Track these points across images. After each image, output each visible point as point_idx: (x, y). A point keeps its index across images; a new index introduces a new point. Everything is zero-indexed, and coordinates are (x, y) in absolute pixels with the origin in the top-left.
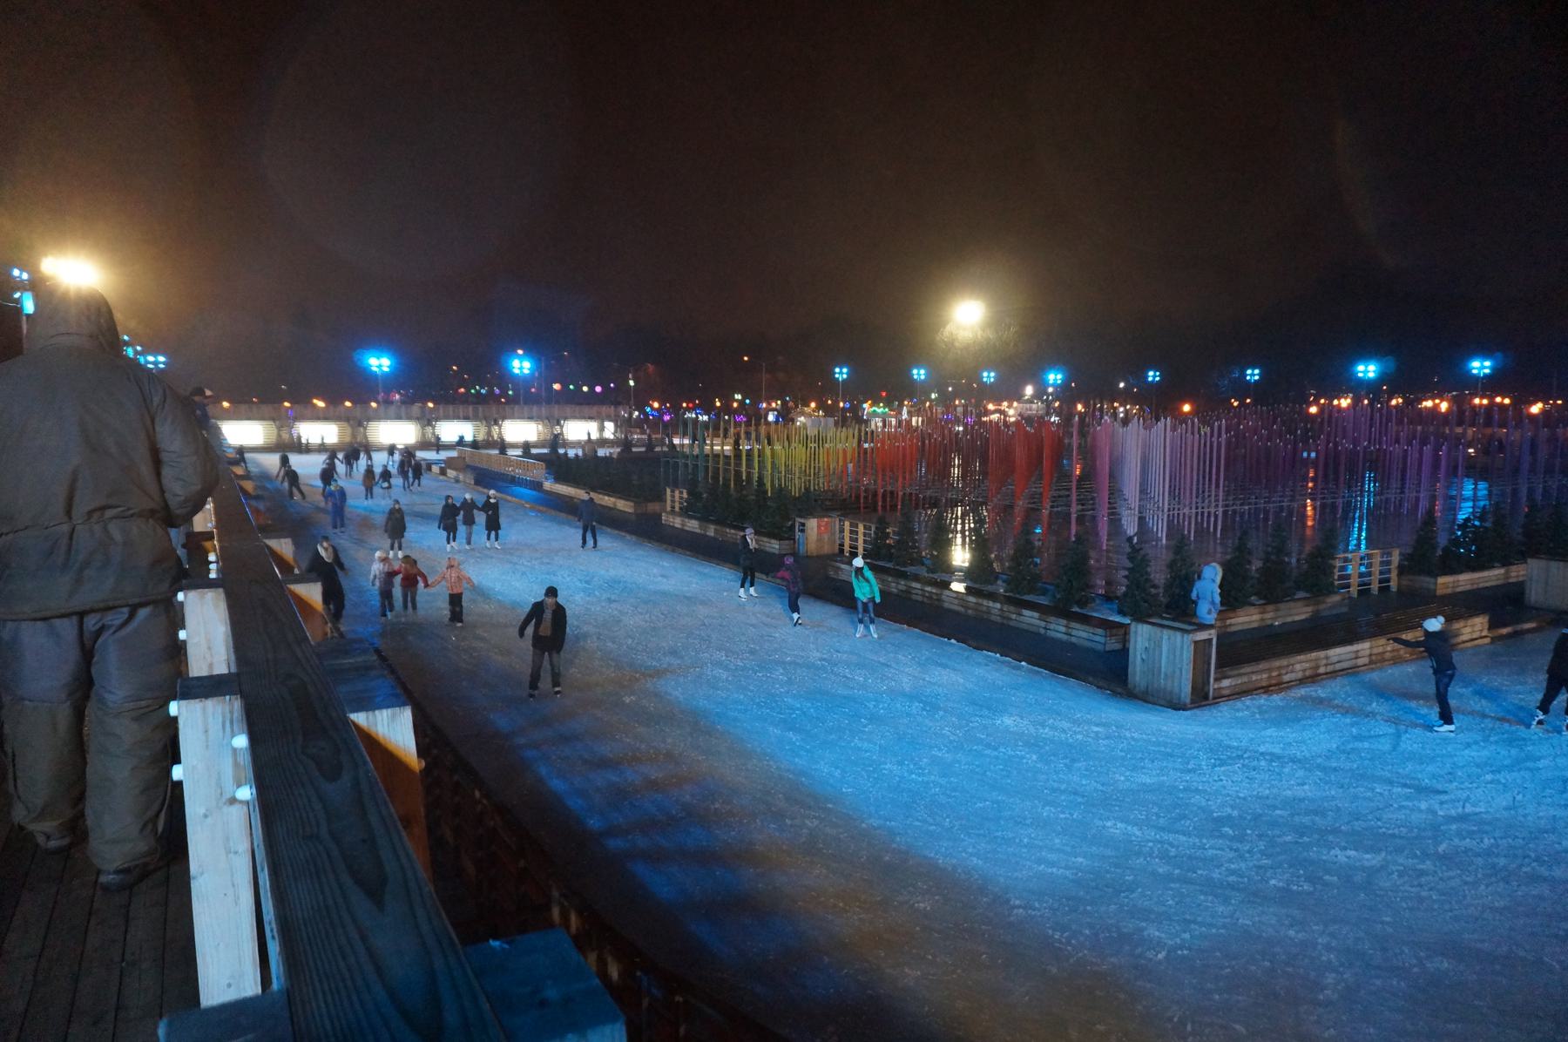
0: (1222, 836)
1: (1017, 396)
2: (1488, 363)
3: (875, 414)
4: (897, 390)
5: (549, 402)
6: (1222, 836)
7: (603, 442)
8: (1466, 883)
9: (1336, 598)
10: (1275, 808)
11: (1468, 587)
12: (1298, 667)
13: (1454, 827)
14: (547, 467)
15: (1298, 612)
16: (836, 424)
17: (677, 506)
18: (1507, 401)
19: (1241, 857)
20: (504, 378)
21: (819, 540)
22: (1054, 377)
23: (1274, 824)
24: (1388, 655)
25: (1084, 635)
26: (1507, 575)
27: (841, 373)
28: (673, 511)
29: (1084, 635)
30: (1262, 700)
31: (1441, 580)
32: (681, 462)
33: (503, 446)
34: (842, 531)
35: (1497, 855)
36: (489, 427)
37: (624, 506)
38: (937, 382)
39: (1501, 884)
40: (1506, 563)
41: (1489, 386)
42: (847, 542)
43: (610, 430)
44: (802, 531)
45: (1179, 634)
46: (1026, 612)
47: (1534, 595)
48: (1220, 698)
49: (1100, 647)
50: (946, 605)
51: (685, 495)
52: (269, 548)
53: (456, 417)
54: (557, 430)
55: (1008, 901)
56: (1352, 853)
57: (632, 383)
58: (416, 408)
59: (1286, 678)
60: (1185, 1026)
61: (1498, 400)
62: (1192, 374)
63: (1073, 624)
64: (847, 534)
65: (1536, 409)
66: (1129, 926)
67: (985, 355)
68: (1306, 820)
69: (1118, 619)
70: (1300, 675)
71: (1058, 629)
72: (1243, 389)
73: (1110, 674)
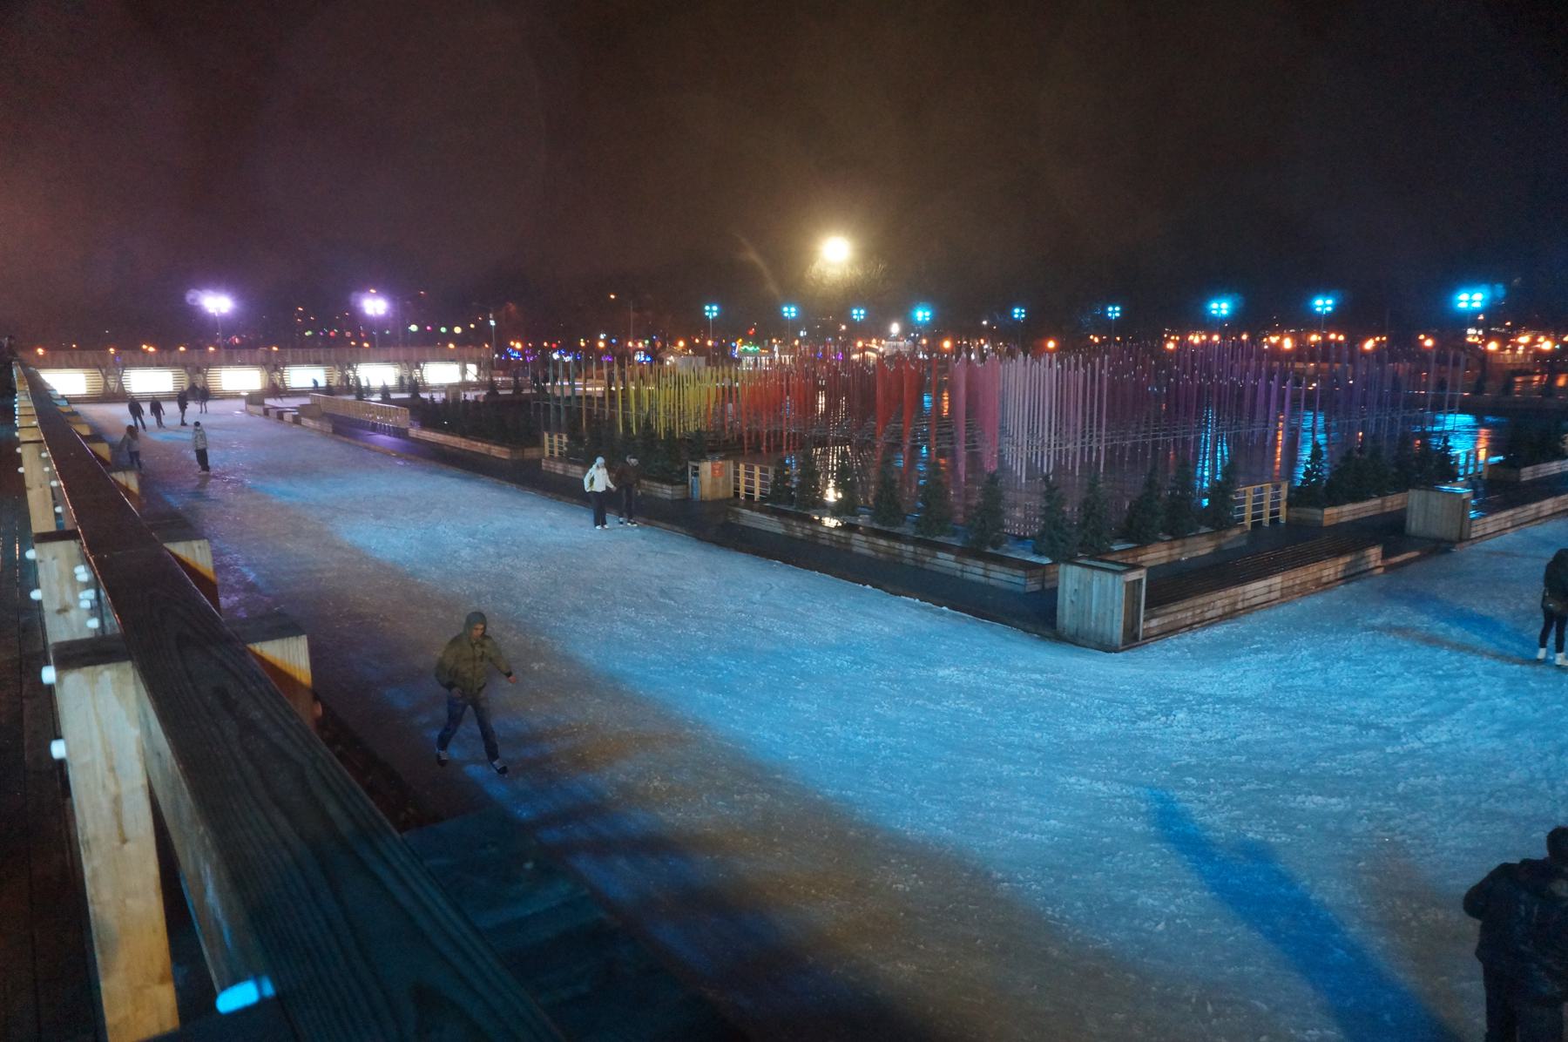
0: (1187, 787)
1: (883, 334)
2: (1330, 302)
3: (746, 353)
4: (768, 328)
5: (405, 344)
6: (1187, 787)
7: (466, 385)
8: (1433, 825)
9: (1236, 532)
10: (1231, 754)
11: (1351, 518)
12: (1219, 603)
13: (1405, 764)
14: (412, 414)
15: (1201, 547)
16: (708, 364)
17: (556, 451)
18: (1341, 338)
19: (1211, 809)
20: (356, 321)
21: (714, 484)
22: (922, 315)
23: (1233, 771)
24: (1297, 589)
25: (1003, 577)
26: (1383, 505)
27: (712, 311)
28: (551, 457)
29: (1003, 577)
30: (1188, 638)
31: (1328, 511)
32: (552, 404)
33: (362, 392)
34: (737, 473)
35: (1455, 793)
36: (342, 371)
37: (498, 452)
38: (804, 320)
39: (1467, 824)
40: (1381, 494)
41: (1329, 322)
42: (742, 486)
43: (472, 372)
44: (696, 475)
45: (1110, 576)
46: (940, 554)
47: (1415, 524)
48: (1150, 637)
49: (1020, 589)
50: (855, 549)
51: (565, 439)
52: (177, 558)
53: (307, 361)
54: (277, 376)
55: (988, 874)
56: (1318, 799)
57: (492, 323)
58: (260, 353)
59: (1208, 615)
60: (1205, 1007)
61: (1332, 336)
62: (1059, 315)
63: (991, 567)
64: (742, 478)
65: (1369, 345)
66: (1120, 895)
67: (853, 294)
68: (1265, 765)
69: (1034, 559)
70: (1220, 612)
71: (975, 571)
72: (1105, 326)
73: (1038, 616)
